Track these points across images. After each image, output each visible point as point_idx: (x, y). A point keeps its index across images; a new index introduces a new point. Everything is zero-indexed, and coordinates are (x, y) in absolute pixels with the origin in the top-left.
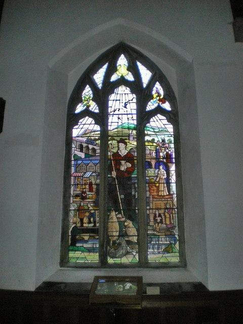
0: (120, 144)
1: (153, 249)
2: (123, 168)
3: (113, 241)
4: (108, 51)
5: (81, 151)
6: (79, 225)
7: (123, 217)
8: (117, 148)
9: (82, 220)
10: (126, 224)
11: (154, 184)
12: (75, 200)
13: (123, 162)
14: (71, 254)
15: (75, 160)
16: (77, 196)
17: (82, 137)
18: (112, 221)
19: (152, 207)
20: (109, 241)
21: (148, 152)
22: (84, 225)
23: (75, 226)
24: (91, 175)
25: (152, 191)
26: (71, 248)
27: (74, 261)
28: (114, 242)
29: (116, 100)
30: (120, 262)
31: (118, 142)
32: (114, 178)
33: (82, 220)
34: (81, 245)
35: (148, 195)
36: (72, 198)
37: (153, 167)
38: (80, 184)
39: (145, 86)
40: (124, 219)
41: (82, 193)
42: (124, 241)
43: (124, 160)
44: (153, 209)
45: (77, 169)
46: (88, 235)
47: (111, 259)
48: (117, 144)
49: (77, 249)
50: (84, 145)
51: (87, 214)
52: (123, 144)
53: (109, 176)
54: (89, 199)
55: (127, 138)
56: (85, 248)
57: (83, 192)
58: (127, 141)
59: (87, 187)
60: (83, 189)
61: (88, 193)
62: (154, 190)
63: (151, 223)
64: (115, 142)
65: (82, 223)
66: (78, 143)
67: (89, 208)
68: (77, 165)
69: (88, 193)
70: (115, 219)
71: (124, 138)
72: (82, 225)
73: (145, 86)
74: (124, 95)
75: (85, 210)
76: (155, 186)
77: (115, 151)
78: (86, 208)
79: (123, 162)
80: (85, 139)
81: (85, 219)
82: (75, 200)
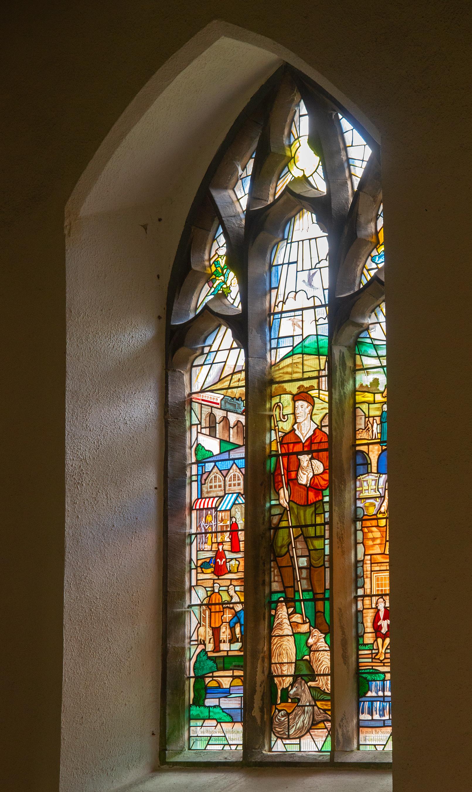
0: (299, 403)
1: (371, 713)
2: (304, 479)
3: (283, 690)
4: (253, 168)
5: (212, 434)
6: (210, 647)
7: (304, 623)
8: (291, 417)
9: (216, 631)
10: (311, 641)
11: (374, 523)
12: (201, 576)
13: (304, 459)
14: (213, 510)
15: (198, 462)
16: (204, 565)
17: (212, 391)
18: (281, 633)
19: (368, 592)
20: (273, 687)
21: (361, 423)
22: (224, 647)
23: (204, 650)
24: (234, 504)
25: (370, 543)
26: (195, 711)
27: (199, 745)
28: (285, 691)
29: (289, 263)
30: (296, 748)
31: (296, 398)
32: (285, 508)
33: (216, 631)
34: (215, 702)
35: (360, 557)
36: (194, 572)
37: (374, 469)
38: (212, 533)
39: (220, 226)
40: (305, 628)
41: (216, 557)
42: (307, 691)
43: (307, 453)
44: (371, 596)
45: (205, 490)
46: (230, 673)
47: (279, 741)
48: (291, 403)
49: (205, 712)
50: (219, 414)
51: (228, 616)
52: (305, 404)
53: (273, 502)
54: (230, 572)
55: (314, 383)
56: (222, 709)
57: (219, 555)
58: (314, 393)
59: (227, 537)
60: (219, 544)
61: (229, 555)
62: (374, 539)
63: (369, 638)
64: (287, 399)
65: (217, 641)
66: (206, 410)
67: (232, 597)
68: (205, 476)
69: (229, 555)
70: (287, 630)
71: (306, 384)
72: (217, 649)
73: (220, 226)
74: (306, 243)
75: (223, 604)
76: (377, 526)
77: (286, 426)
78: (225, 597)
79: (304, 459)
80: (218, 397)
81: (223, 629)
82: (201, 576)
